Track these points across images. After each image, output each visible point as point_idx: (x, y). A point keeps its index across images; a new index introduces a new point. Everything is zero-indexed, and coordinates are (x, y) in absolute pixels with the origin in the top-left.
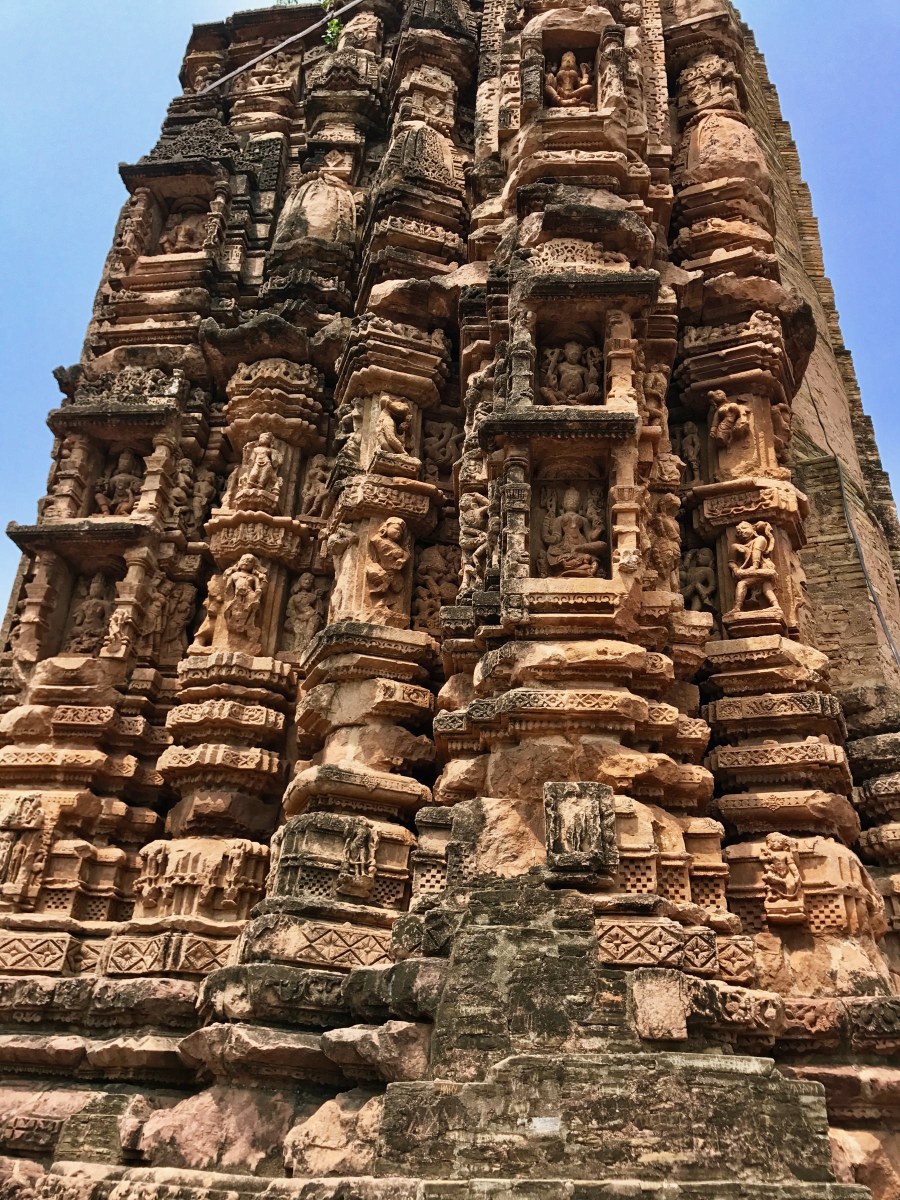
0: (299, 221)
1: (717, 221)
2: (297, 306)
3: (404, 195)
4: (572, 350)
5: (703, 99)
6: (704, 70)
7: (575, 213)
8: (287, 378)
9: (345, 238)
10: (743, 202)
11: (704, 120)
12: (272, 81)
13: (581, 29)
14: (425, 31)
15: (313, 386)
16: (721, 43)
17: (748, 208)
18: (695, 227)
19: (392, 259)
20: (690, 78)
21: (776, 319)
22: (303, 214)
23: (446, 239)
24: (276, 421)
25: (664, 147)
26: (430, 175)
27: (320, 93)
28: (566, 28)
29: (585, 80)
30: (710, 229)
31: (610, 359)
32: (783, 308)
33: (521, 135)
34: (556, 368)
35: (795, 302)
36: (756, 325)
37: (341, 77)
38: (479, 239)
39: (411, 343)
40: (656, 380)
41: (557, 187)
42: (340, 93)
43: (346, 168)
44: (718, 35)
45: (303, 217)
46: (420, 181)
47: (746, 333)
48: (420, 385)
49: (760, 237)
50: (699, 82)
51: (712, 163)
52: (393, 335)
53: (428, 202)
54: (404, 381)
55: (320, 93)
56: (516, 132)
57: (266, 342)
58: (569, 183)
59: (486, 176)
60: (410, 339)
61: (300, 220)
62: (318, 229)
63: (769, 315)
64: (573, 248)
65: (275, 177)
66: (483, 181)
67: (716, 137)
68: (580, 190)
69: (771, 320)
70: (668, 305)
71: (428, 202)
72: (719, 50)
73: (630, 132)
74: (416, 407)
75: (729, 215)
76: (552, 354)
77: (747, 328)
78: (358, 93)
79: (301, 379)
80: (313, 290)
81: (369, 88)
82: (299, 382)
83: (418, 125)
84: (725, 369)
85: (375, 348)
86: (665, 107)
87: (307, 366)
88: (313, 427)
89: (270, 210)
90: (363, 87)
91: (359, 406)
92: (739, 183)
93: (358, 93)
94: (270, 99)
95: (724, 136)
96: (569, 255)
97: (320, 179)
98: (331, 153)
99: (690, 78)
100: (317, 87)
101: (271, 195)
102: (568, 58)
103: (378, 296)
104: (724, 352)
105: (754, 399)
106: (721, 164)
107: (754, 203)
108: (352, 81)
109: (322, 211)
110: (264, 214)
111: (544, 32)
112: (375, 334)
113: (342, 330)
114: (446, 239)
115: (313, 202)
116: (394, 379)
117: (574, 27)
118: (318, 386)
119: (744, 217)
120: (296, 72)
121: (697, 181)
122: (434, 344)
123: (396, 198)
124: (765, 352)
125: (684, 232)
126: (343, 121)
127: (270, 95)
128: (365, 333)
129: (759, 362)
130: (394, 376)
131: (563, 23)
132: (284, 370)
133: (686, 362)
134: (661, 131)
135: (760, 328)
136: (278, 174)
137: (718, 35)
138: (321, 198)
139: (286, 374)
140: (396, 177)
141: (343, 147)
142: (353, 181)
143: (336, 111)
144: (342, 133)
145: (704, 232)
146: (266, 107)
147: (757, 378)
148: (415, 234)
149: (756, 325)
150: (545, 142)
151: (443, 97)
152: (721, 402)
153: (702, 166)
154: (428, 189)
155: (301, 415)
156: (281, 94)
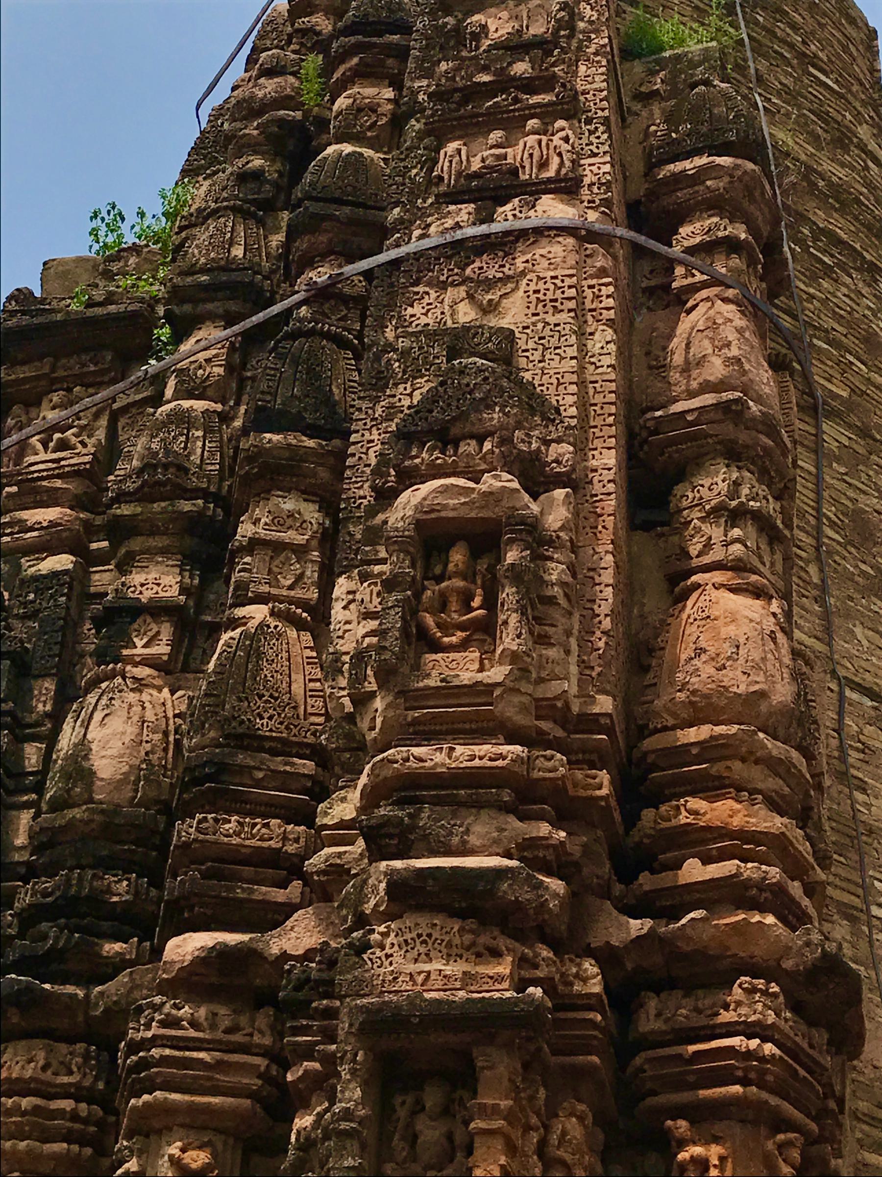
0: (79, 769)
1: (694, 803)
2: (68, 940)
3: (222, 769)
4: (432, 1097)
5: (699, 546)
6: (704, 492)
7: (431, 882)
8: (48, 1076)
9: (152, 794)
10: (737, 765)
11: (695, 595)
12: (63, 445)
13: (473, 515)
14: (276, 438)
15: (87, 1083)
16: (734, 442)
17: (745, 775)
18: (663, 808)
19: (196, 895)
20: (685, 503)
21: (775, 988)
22: (86, 757)
23: (285, 838)
24: (29, 1152)
25: (600, 698)
26: (265, 726)
27: (126, 510)
28: (451, 514)
29: (477, 602)
30: (684, 818)
31: (471, 1136)
32: (788, 964)
33: (378, 703)
34: (410, 1125)
35: (807, 951)
36: (739, 1004)
37: (159, 483)
38: (318, 873)
39: (220, 1042)
40: (564, 1133)
41: (420, 810)
42: (157, 507)
43: (162, 649)
44: (728, 430)
45: (85, 764)
46: (248, 740)
47: (726, 1017)
48: (233, 1112)
49: (763, 826)
50: (697, 514)
51: (694, 692)
52: (192, 1033)
53: (260, 775)
54: (207, 1109)
55: (126, 510)
56: (372, 695)
57: (15, 1020)
58: (436, 802)
59: (337, 749)
60: (219, 1035)
61: (82, 769)
62: (110, 782)
63: (760, 983)
64: (429, 935)
65: (56, 649)
66: (335, 757)
67: (703, 644)
68: (454, 815)
69: (765, 993)
70: (589, 995)
71: (260, 775)
72: (734, 455)
73: (540, 692)
74: (231, 1141)
75: (712, 788)
76: (403, 1103)
77: (726, 1007)
78: (186, 506)
79: (70, 1073)
80: (96, 901)
81: (205, 494)
82: (66, 1079)
83: (258, 613)
84: (691, 1078)
85: (164, 1061)
86: (607, 624)
87: (80, 1047)
88: (88, 1151)
89: (47, 715)
90: (192, 494)
91: (141, 1153)
92: (727, 736)
93: (186, 506)
94: (58, 483)
95: (716, 638)
96: (423, 950)
97: (119, 680)
98: (140, 621)
99: (685, 503)
100: (122, 497)
101: (49, 685)
102: (458, 557)
103: (173, 962)
104: (692, 1048)
105: (737, 1129)
106: (706, 696)
107: (756, 762)
108: (177, 486)
109: (116, 747)
110: (37, 724)
111: (419, 524)
112: (163, 1037)
113: (131, 991)
114: (285, 838)
115: (107, 731)
116: (192, 1108)
117: (464, 512)
118: (97, 1079)
119: (739, 789)
120: (103, 422)
121: (671, 722)
122: (256, 1039)
123: (209, 778)
124: (749, 1055)
125: (648, 814)
126: (164, 551)
127: (58, 476)
128: (149, 1034)
129: (740, 1073)
130: (191, 1106)
131: (445, 507)
132: (41, 1063)
133: (638, 1061)
134: (598, 669)
135: (743, 1010)
136: (62, 644)
137: (728, 430)
138: (117, 723)
139: (44, 1068)
140: (212, 734)
141: (158, 610)
142: (172, 671)
143: (152, 534)
144: (159, 581)
145: (674, 822)
146: (50, 499)
147: (734, 1101)
148: (235, 840)
149: (739, 1004)
150: (410, 724)
151: (301, 551)
152: (682, 1144)
153: (681, 696)
154: (261, 749)
155: (68, 1138)
156: (76, 473)
